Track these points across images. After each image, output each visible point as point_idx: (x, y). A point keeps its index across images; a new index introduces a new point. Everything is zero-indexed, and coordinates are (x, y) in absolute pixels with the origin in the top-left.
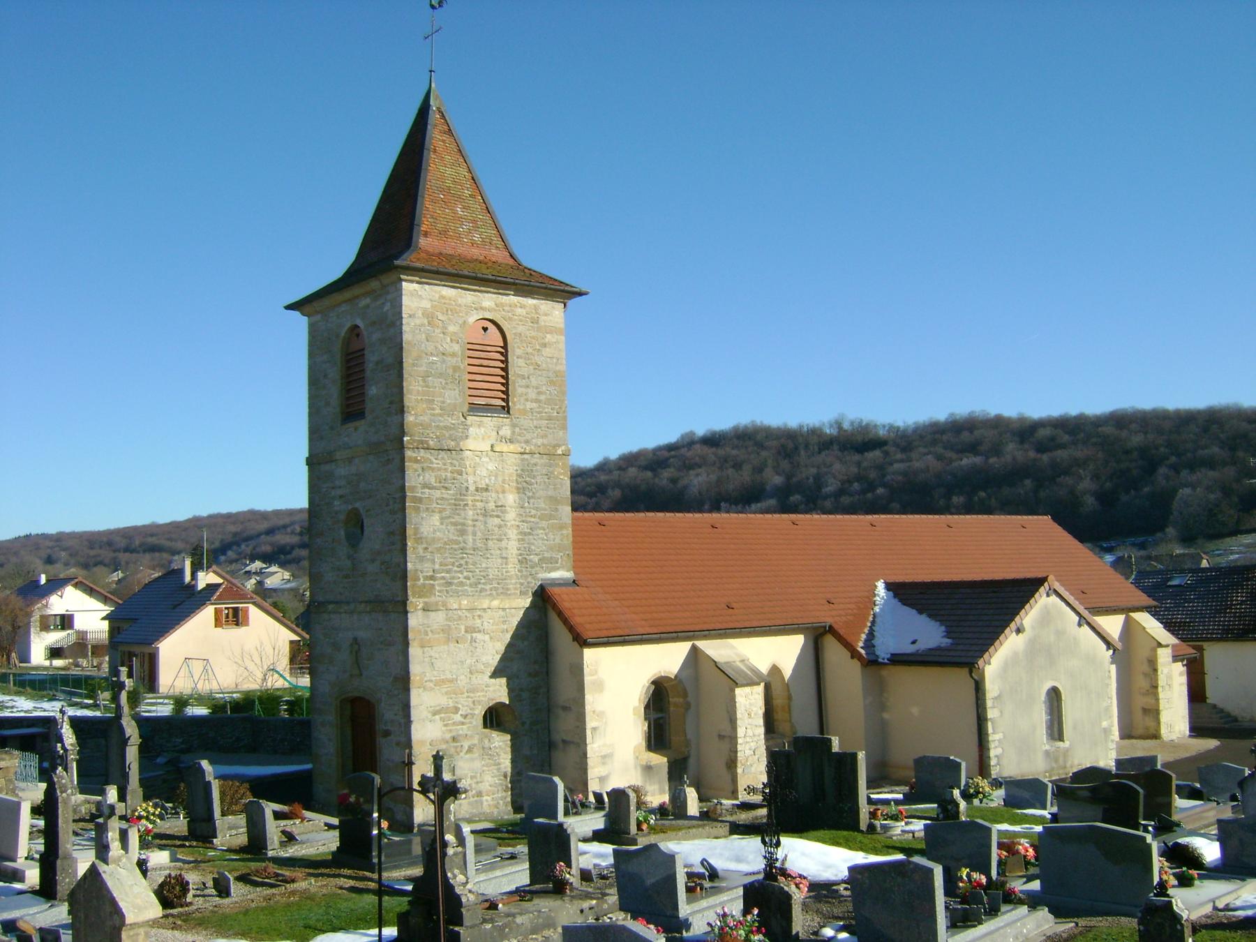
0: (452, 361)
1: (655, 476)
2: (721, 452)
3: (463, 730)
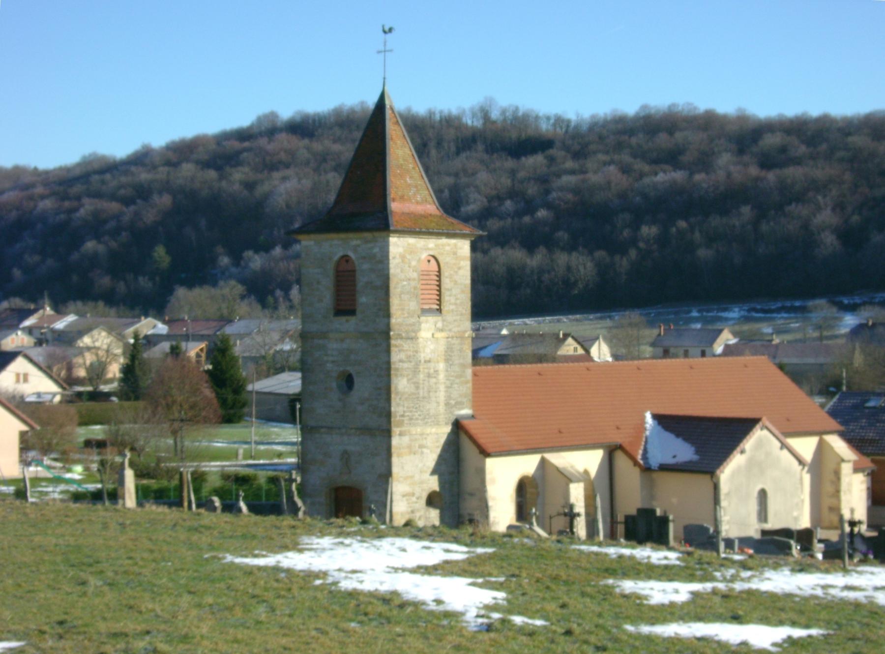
0: (413, 283)
1: (221, 178)
2: (317, 147)
3: (417, 506)
